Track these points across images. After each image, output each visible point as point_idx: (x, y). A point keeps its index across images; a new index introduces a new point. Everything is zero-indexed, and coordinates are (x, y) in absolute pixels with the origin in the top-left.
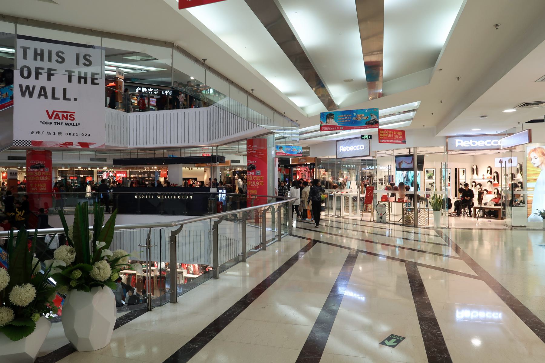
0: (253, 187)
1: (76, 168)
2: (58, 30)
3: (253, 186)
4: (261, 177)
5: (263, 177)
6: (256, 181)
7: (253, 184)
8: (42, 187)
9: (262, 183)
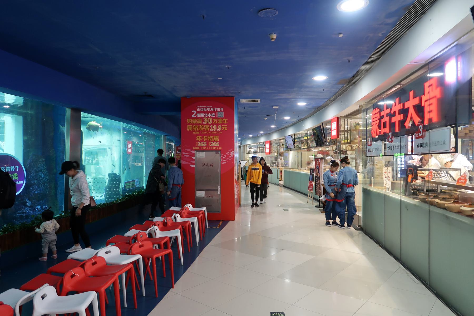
0: (213, 133)
1: (414, 93)
2: (15, 144)
3: (213, 131)
4: (225, 119)
5: (226, 120)
6: (217, 125)
7: (213, 129)
8: (213, 142)
9: (225, 128)
